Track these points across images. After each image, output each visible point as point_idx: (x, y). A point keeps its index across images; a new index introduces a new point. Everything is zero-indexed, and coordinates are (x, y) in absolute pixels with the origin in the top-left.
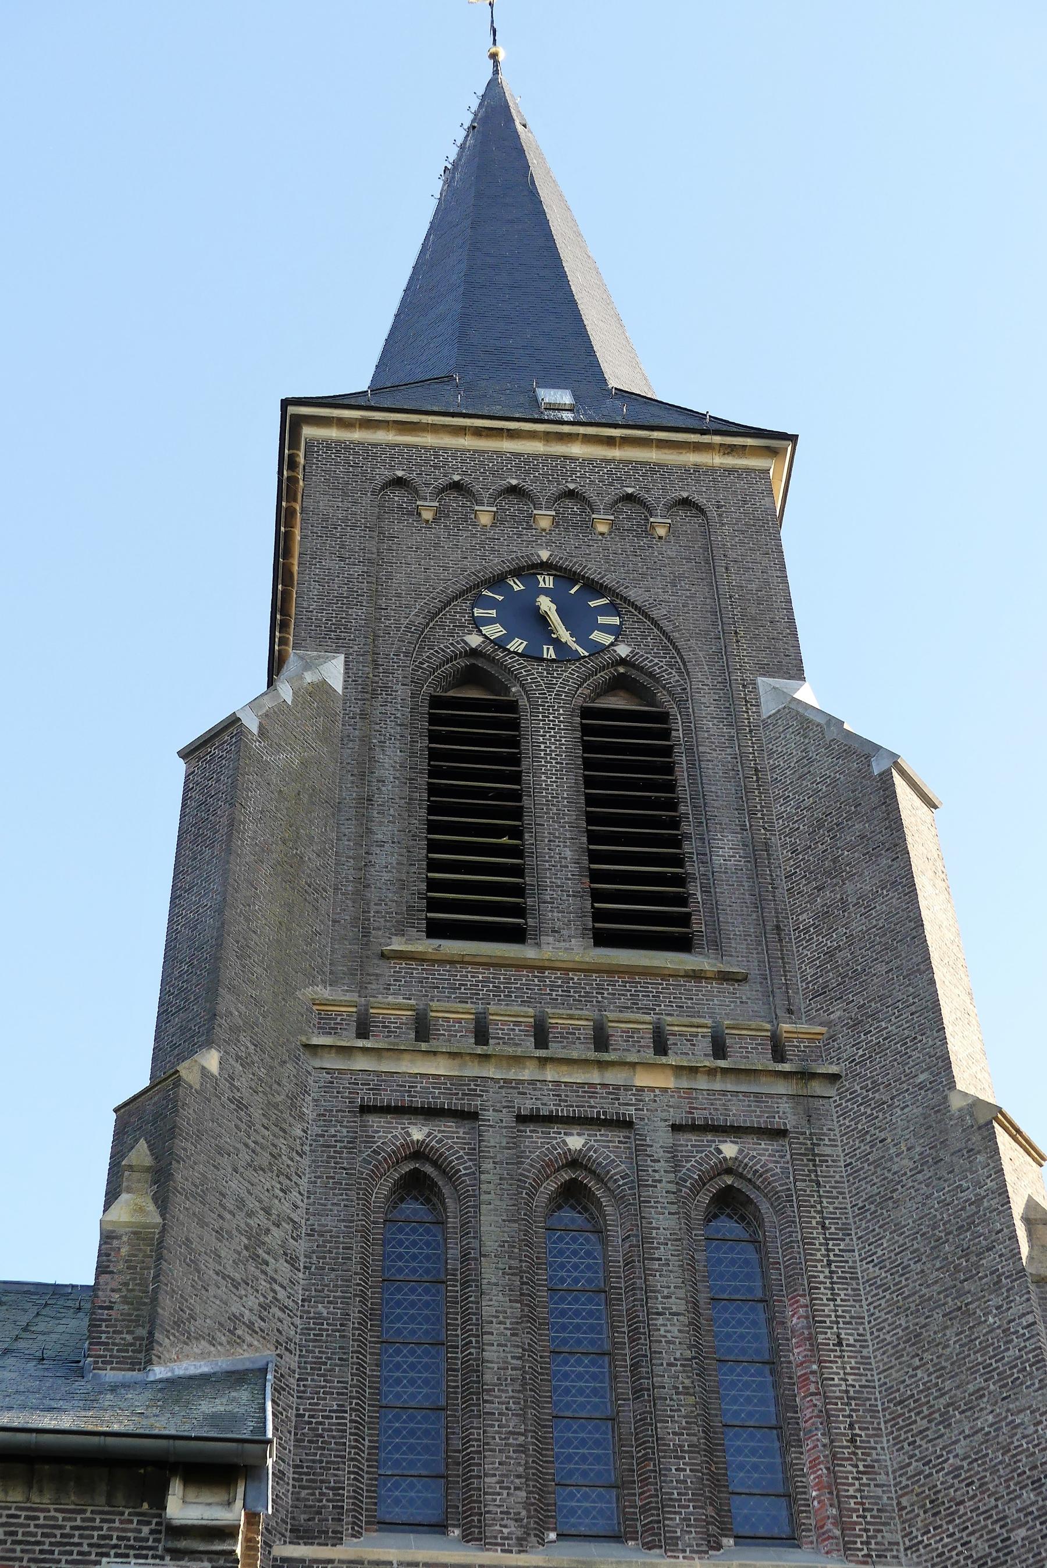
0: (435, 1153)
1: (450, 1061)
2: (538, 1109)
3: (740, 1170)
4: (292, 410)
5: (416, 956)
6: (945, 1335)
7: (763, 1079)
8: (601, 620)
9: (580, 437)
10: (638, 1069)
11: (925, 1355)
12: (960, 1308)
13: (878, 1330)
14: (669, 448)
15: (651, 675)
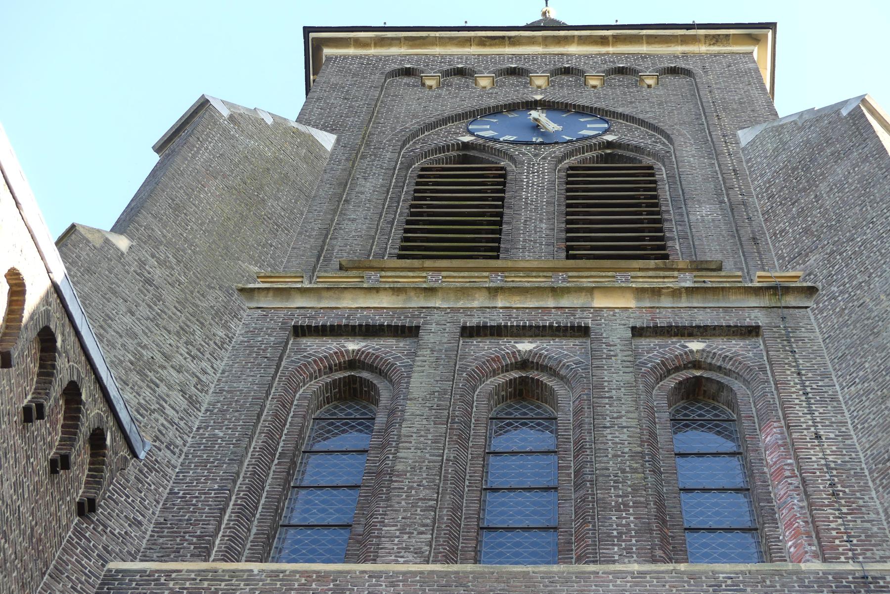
0: (371, 358)
1: (394, 297)
2: (487, 323)
4: (312, 35)
8: (588, 126)
9: (576, 39)
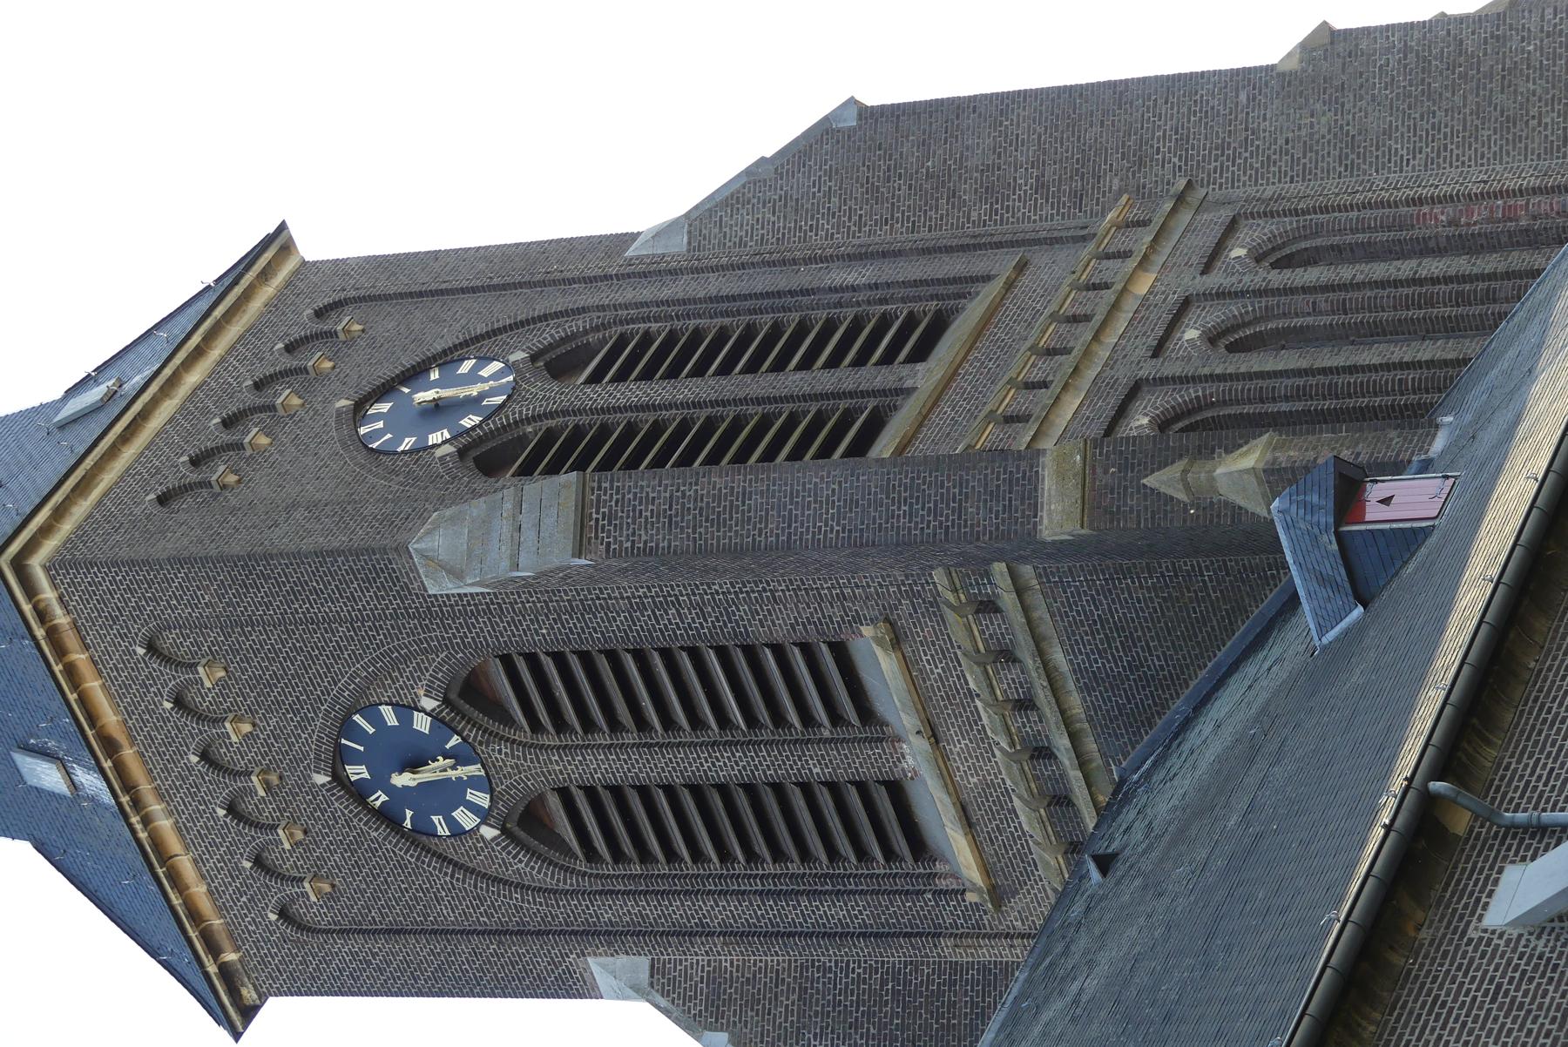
3: (1261, 251)
5: (905, 442)
6: (1522, 93)
7: (1172, 224)
10: (1130, 288)
11: (1531, 113)
12: (1504, 77)
13: (1482, 158)
14: (234, 315)
15: (563, 340)
